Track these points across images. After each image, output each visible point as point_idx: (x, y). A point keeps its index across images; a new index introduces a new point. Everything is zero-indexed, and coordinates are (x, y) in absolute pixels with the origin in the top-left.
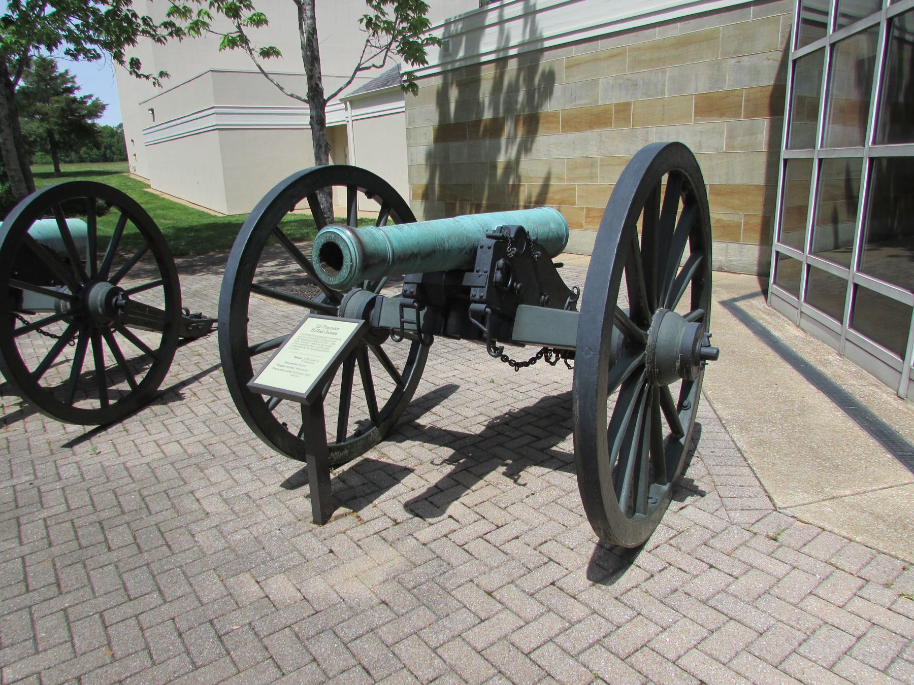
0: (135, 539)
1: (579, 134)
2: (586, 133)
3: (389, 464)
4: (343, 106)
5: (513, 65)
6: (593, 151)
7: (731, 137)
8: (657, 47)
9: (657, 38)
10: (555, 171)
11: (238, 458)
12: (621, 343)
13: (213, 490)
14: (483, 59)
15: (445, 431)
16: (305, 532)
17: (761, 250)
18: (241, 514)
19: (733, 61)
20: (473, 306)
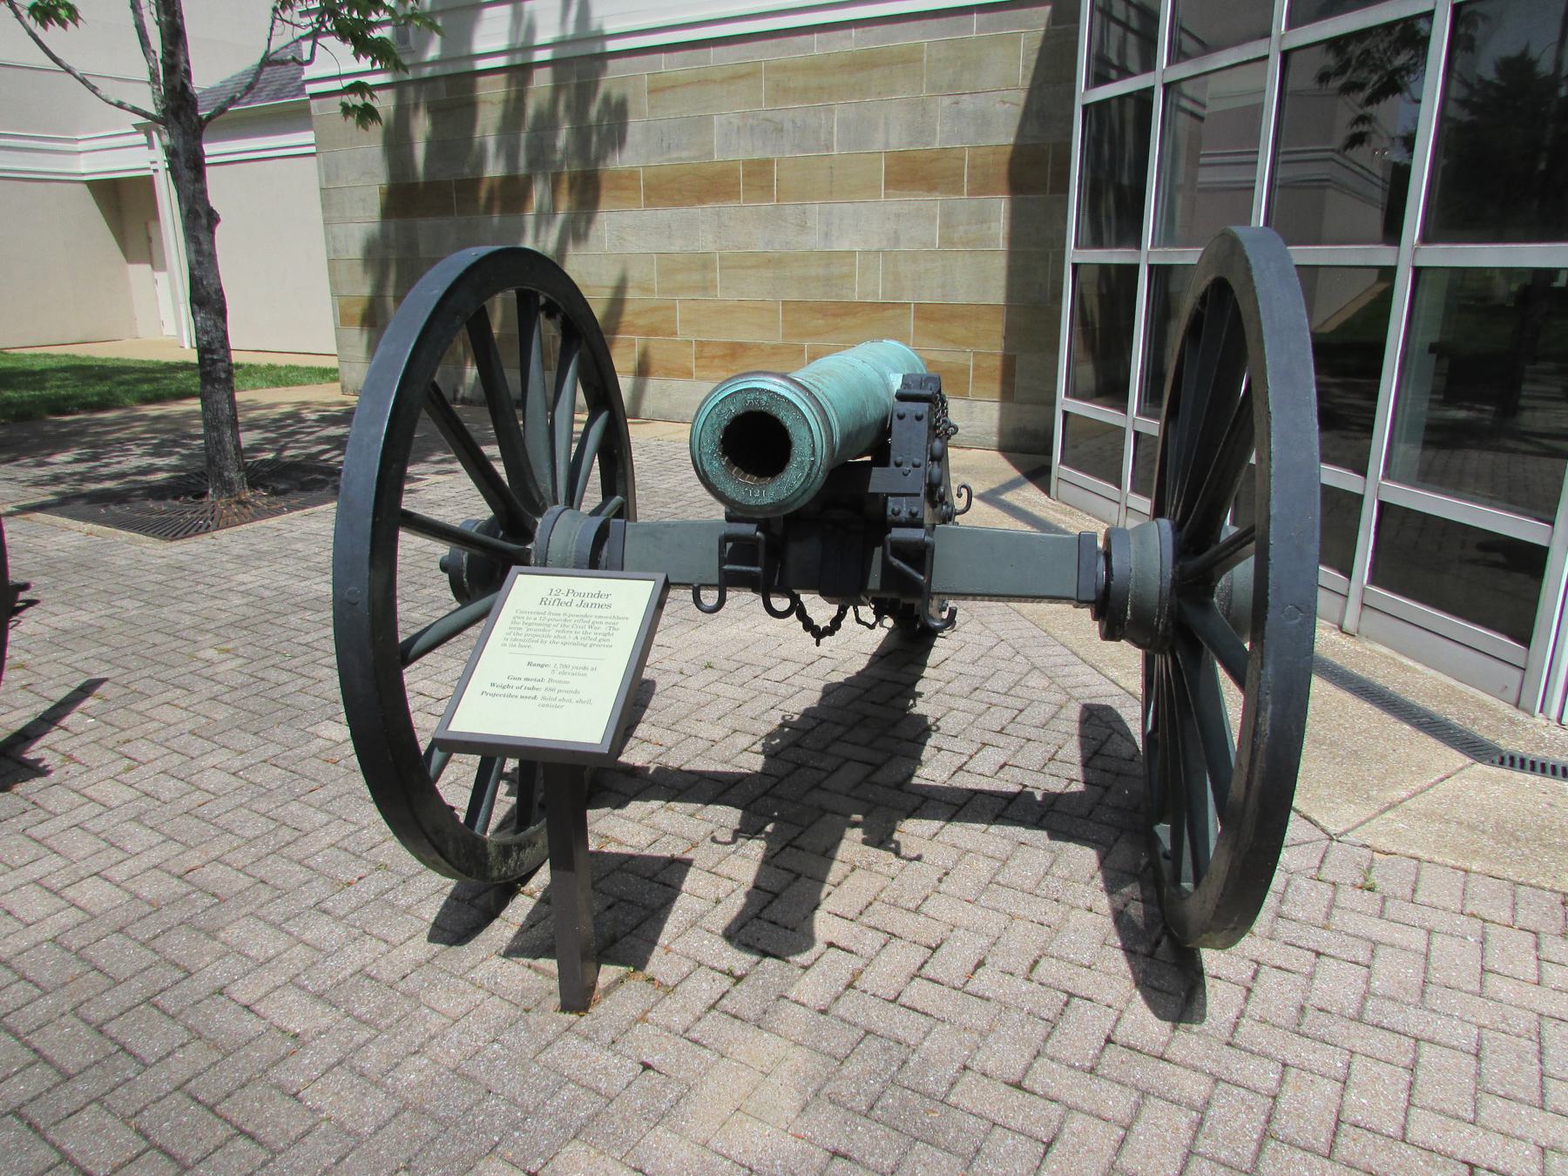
0: (146, 1137)
1: (683, 211)
2: (691, 210)
3: (632, 857)
4: (142, 138)
5: (542, 81)
6: (706, 242)
7: (948, 223)
8: (817, 67)
9: (816, 52)
10: (634, 275)
11: (280, 893)
12: (1167, 585)
13: (270, 978)
14: (481, 65)
15: (691, 772)
16: (559, 1036)
17: (1002, 409)
18: (383, 1023)
19: (946, 101)
20: (897, 534)
